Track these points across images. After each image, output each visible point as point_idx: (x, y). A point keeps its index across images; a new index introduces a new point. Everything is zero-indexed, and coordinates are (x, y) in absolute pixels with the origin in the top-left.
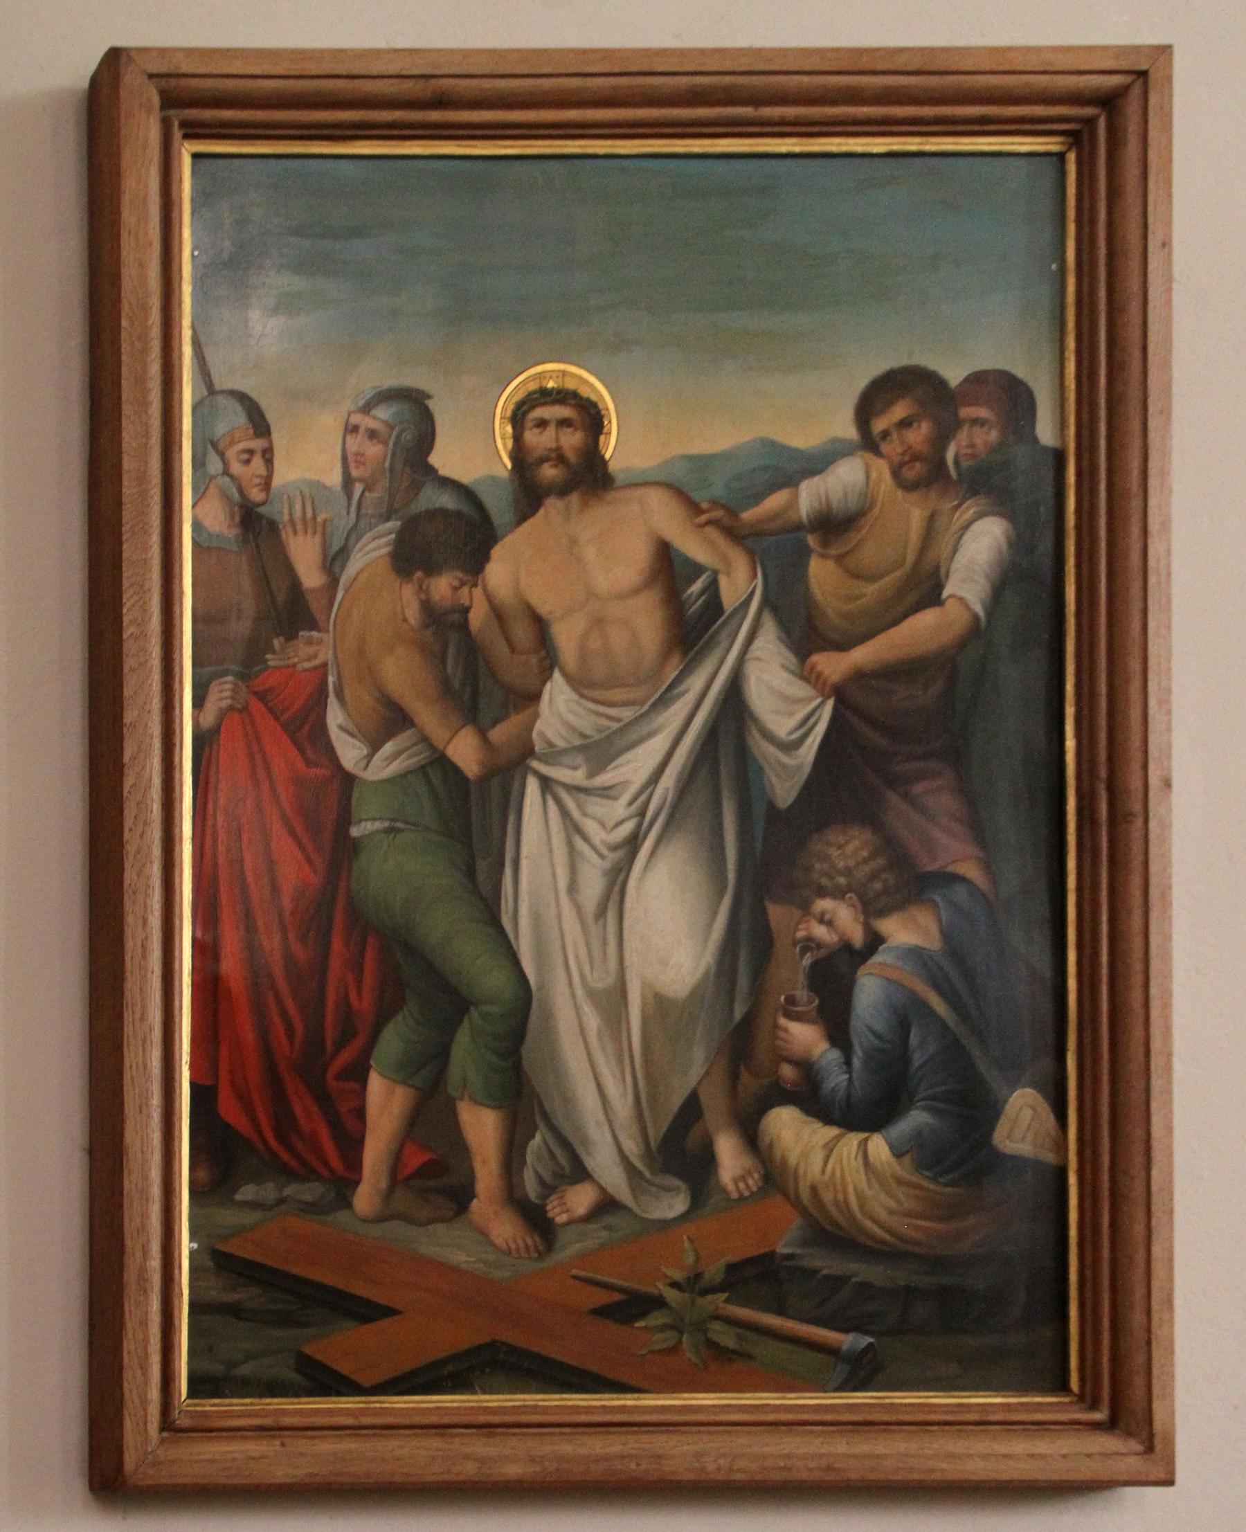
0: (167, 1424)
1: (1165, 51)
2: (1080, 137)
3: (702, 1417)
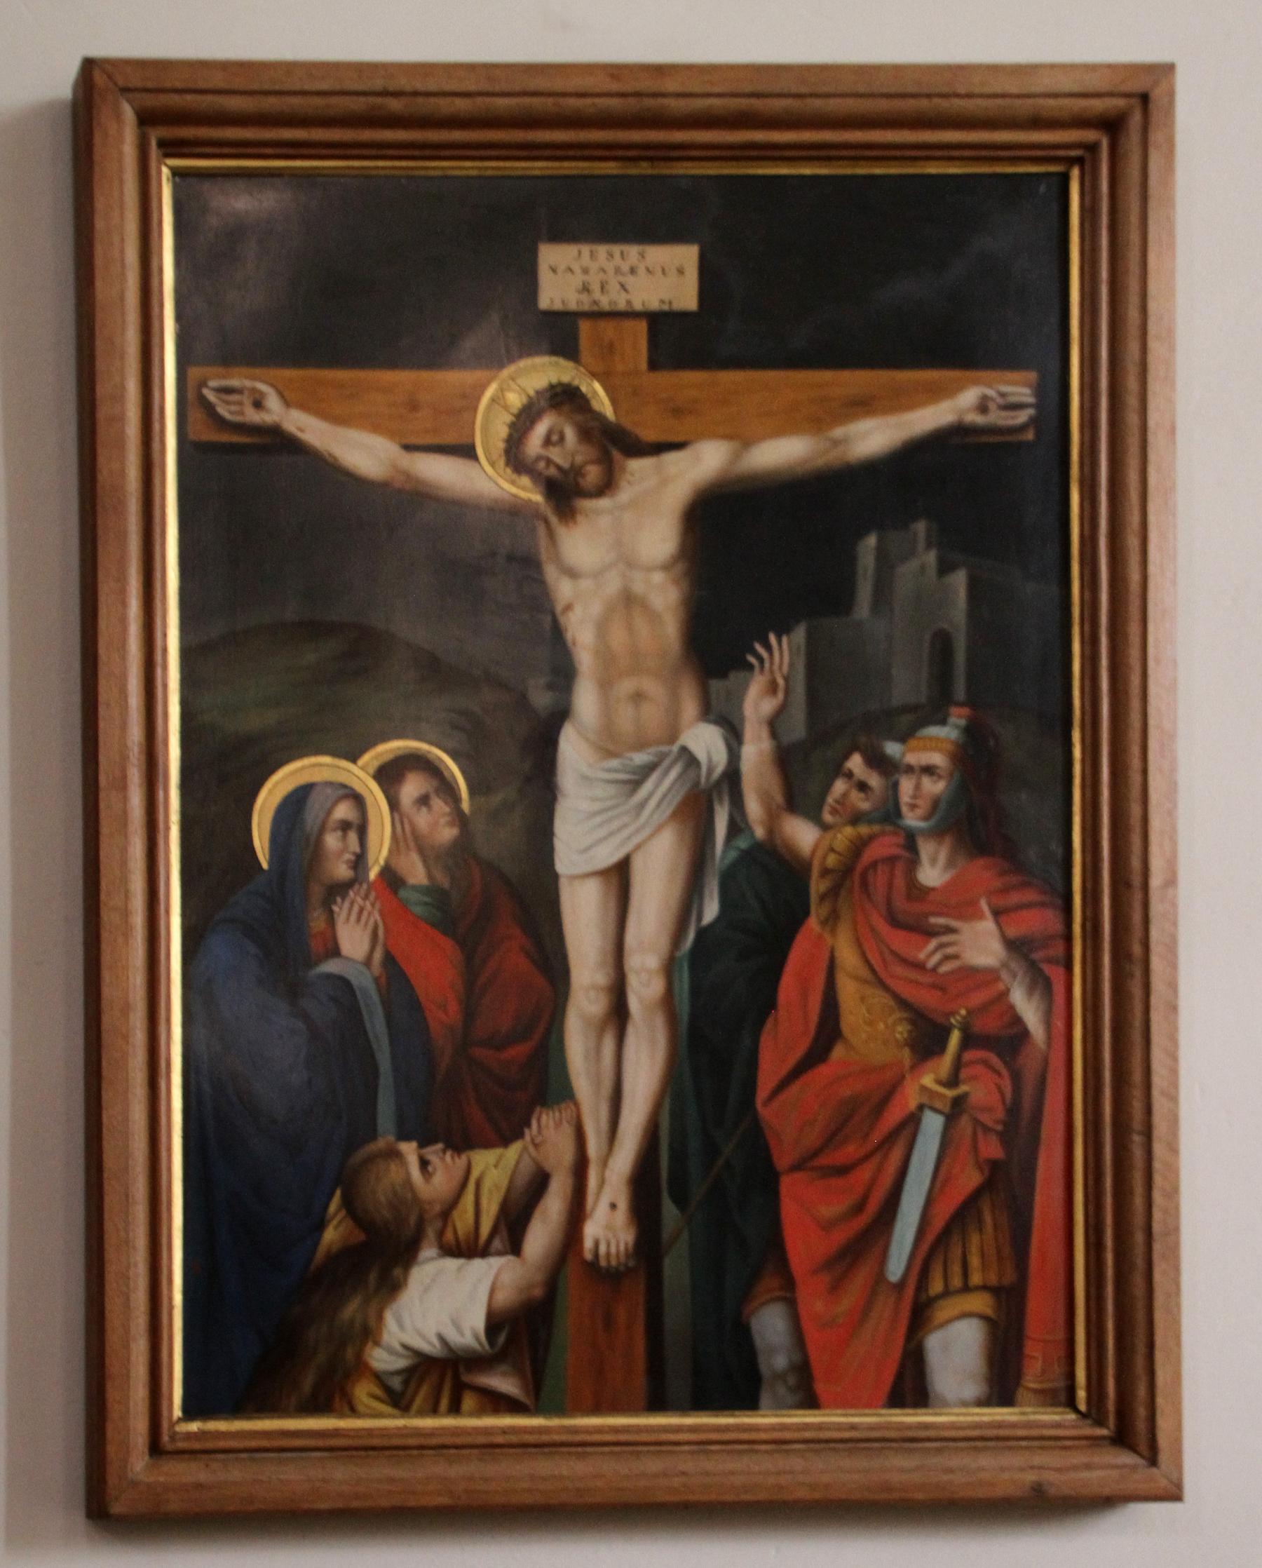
0: (155, 1448)
3: (222, 1444)
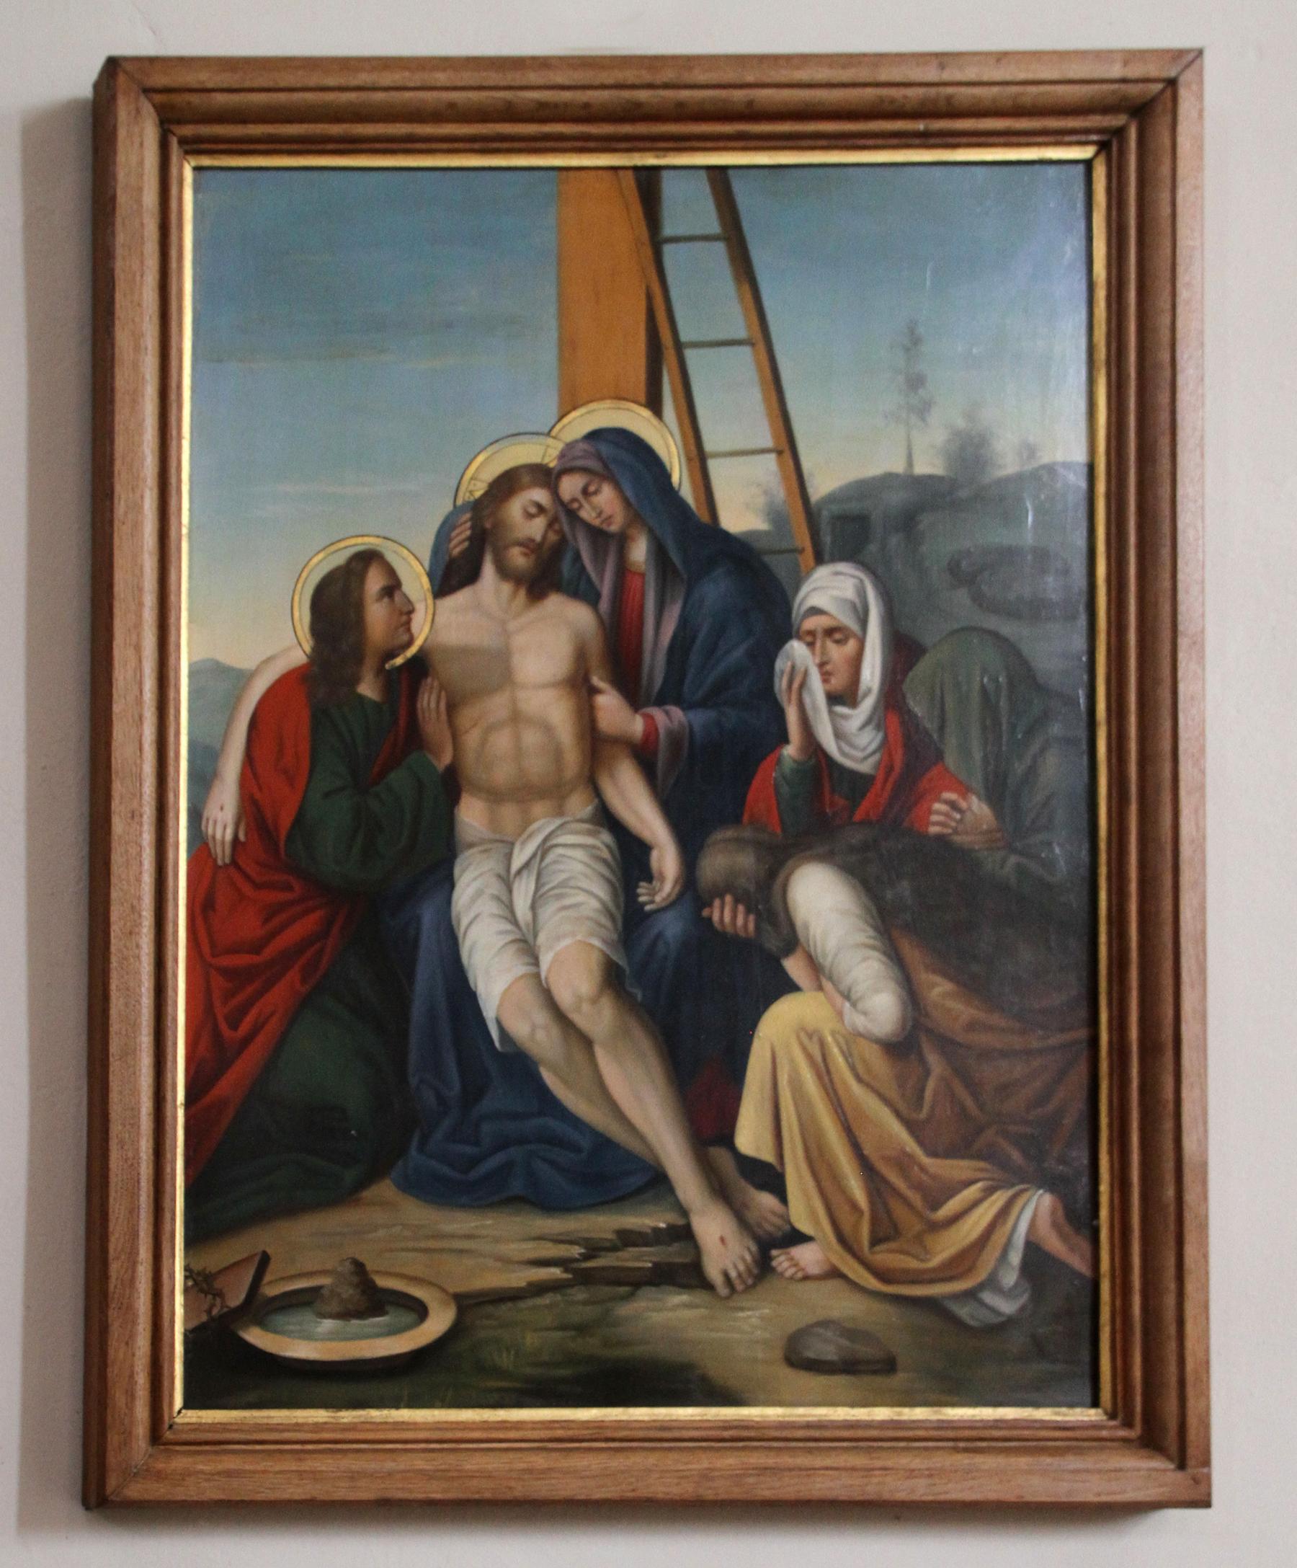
0: (156, 1436)
1: (1191, 58)
2: (1109, 144)
